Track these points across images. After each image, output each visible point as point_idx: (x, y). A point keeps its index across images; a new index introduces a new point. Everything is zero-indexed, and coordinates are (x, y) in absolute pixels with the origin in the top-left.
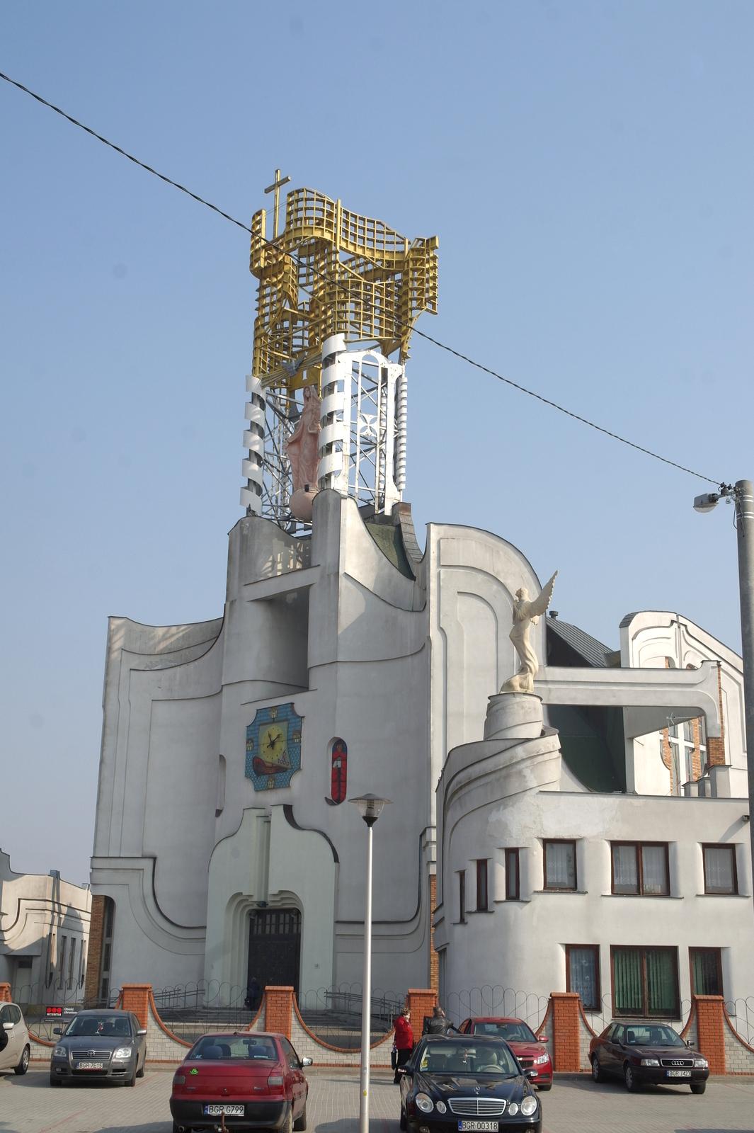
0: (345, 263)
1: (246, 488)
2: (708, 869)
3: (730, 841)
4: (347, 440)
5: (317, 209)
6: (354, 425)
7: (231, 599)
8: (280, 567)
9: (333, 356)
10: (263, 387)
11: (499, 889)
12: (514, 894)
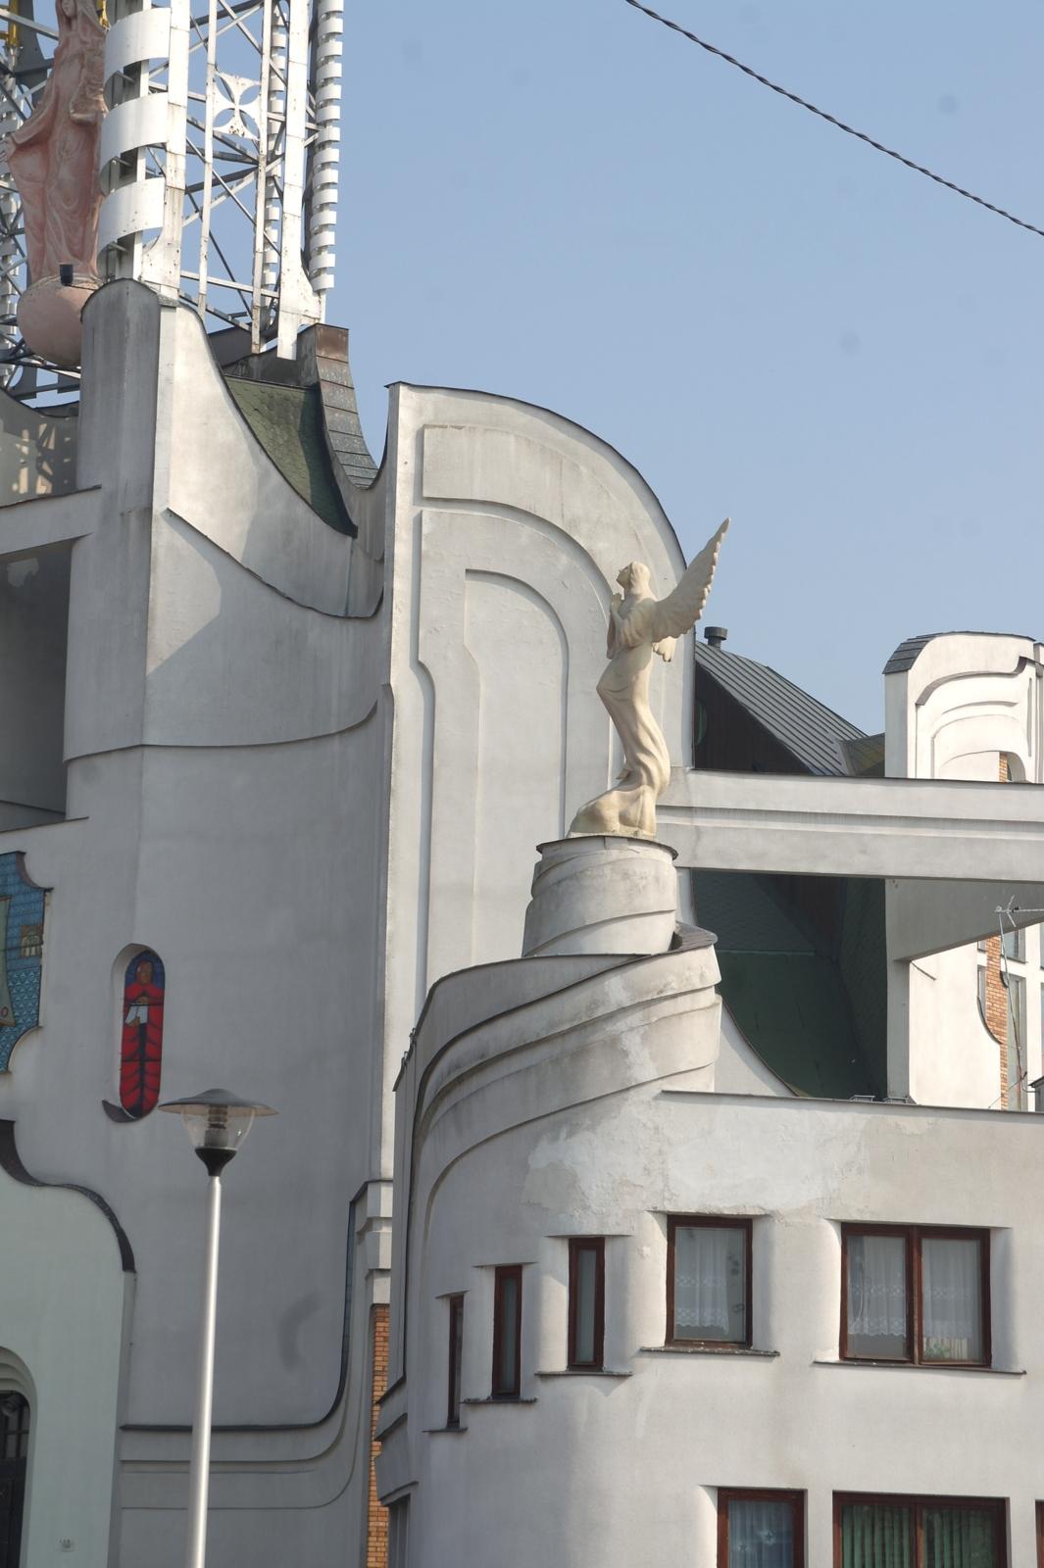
4: (178, 145)
6: (196, 103)
11: (553, 1348)
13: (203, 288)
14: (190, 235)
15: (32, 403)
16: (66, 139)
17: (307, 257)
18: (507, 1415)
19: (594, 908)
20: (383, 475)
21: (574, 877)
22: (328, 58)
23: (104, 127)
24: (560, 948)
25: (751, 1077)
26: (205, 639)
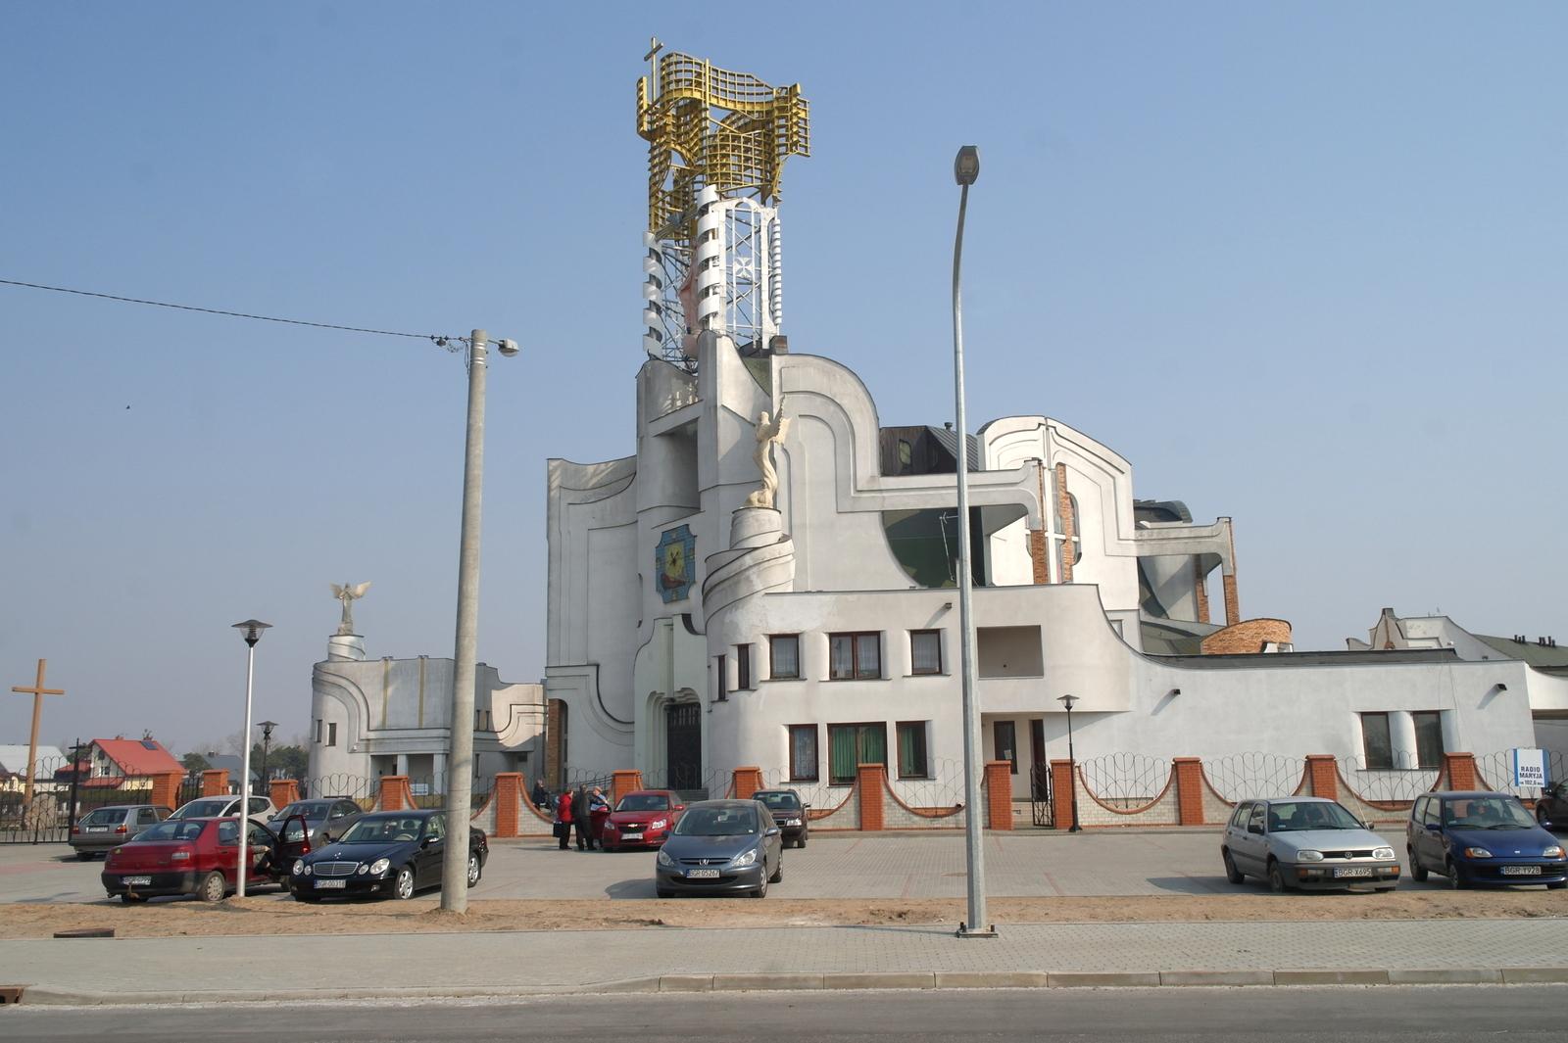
0: (723, 122)
1: (648, 335)
2: (775, 657)
3: (933, 627)
4: (724, 283)
5: (686, 71)
6: (729, 268)
7: (640, 436)
8: (679, 403)
9: (706, 206)
10: (657, 241)
11: (733, 682)
12: (745, 684)
22: (776, 247)
26: (737, 446)
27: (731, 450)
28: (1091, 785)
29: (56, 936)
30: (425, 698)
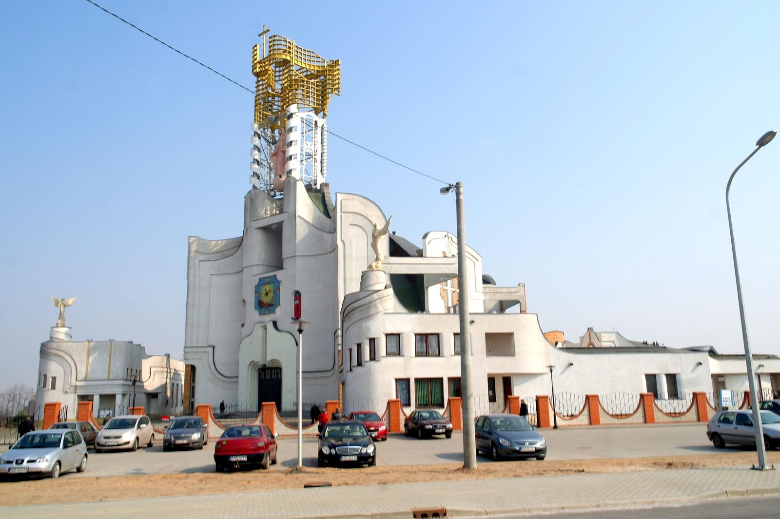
0: (297, 71)
6: (302, 147)
9: (292, 114)
12: (373, 358)
13: (304, 177)
14: (301, 169)
15: (275, 198)
16: (280, 154)
17: (321, 171)
18: (360, 368)
19: (371, 282)
20: (335, 208)
21: (368, 277)
23: (286, 152)
24: (366, 289)
25: (401, 309)
26: (306, 237)
27: (302, 240)
28: (605, 407)
29: (306, 486)
30: (112, 363)
